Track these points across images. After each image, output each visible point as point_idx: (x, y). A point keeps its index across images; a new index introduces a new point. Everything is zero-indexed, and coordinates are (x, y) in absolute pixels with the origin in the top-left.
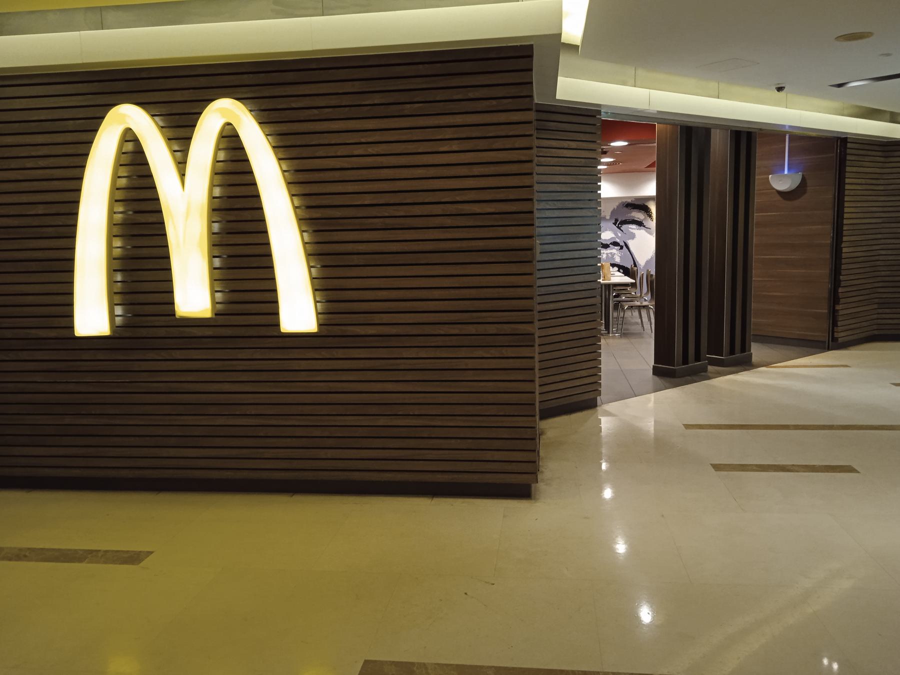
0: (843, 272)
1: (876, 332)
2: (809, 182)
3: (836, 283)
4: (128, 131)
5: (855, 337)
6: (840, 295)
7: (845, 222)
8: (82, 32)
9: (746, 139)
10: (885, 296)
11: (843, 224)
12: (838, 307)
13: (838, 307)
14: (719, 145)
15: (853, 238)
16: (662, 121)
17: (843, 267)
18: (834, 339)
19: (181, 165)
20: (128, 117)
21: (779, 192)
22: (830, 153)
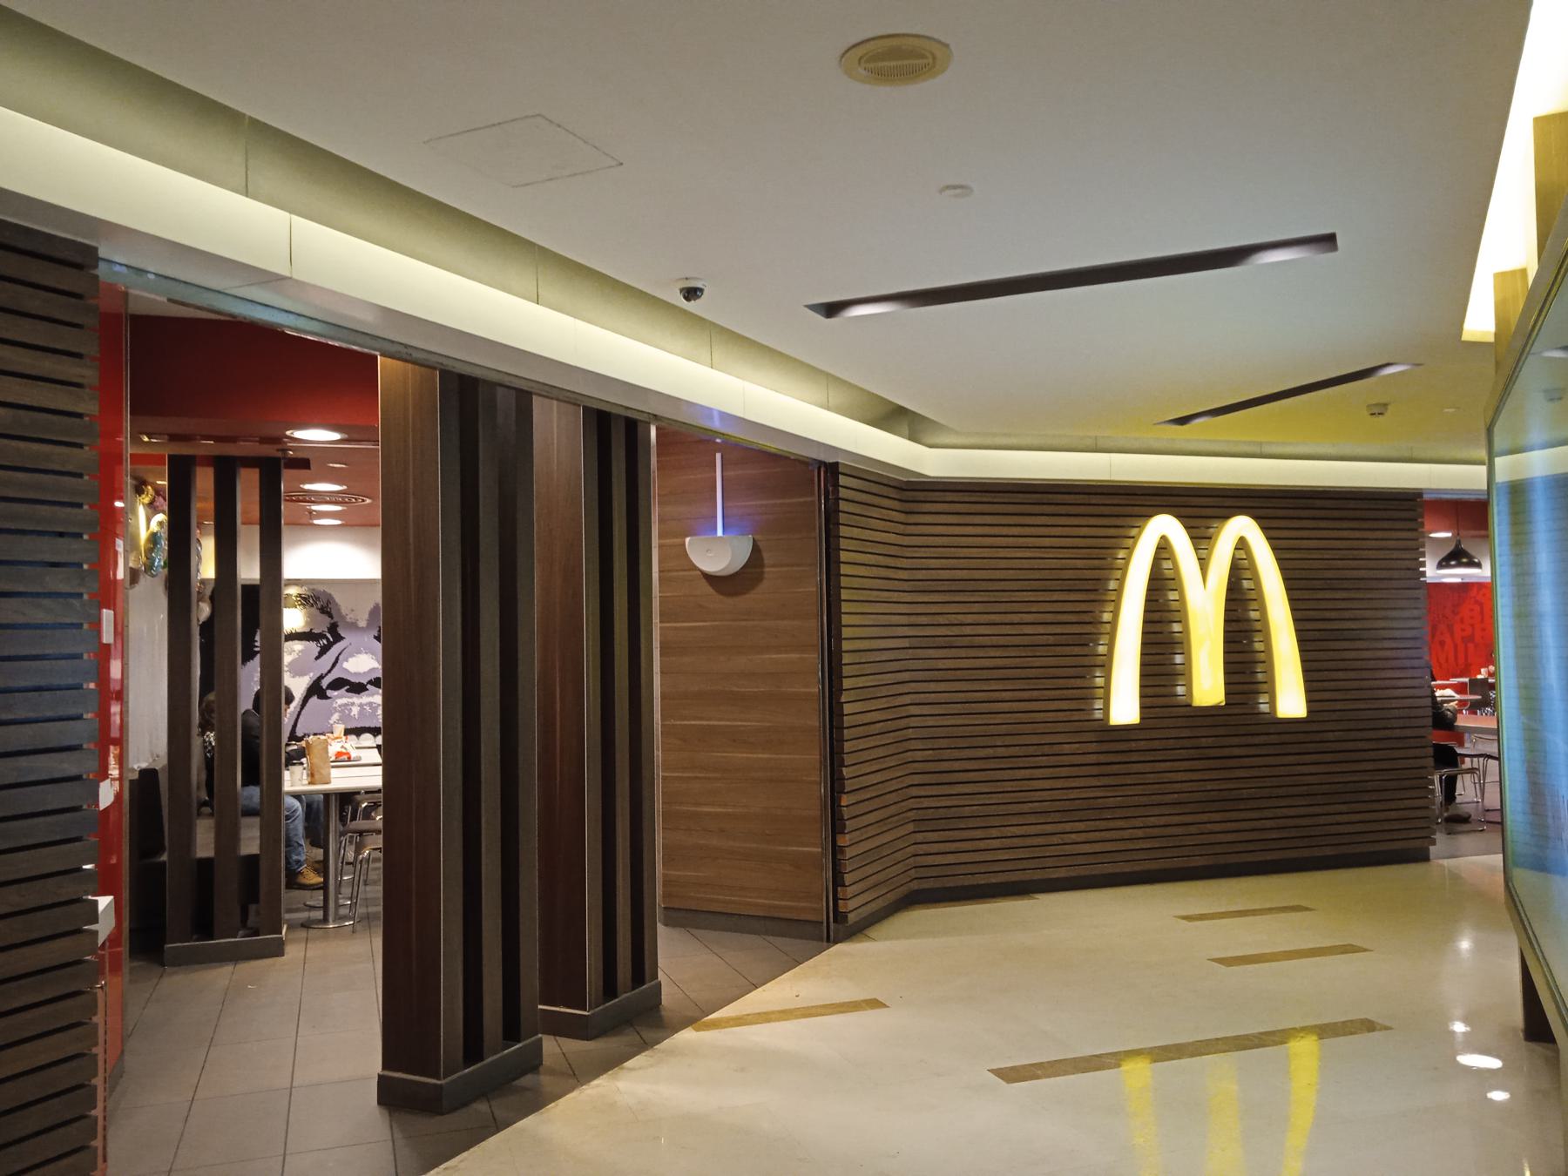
0: (848, 760)
1: (915, 885)
2: (767, 557)
3: (836, 785)
4: (1163, 538)
5: (880, 903)
6: (846, 813)
7: (846, 646)
8: (298, 220)
9: (619, 435)
10: (926, 803)
11: (840, 652)
12: (843, 840)
13: (843, 840)
14: (557, 443)
15: (861, 682)
16: (402, 354)
17: (847, 746)
18: (840, 917)
19: (1204, 563)
20: (1164, 526)
21: (709, 577)
22: (807, 490)
